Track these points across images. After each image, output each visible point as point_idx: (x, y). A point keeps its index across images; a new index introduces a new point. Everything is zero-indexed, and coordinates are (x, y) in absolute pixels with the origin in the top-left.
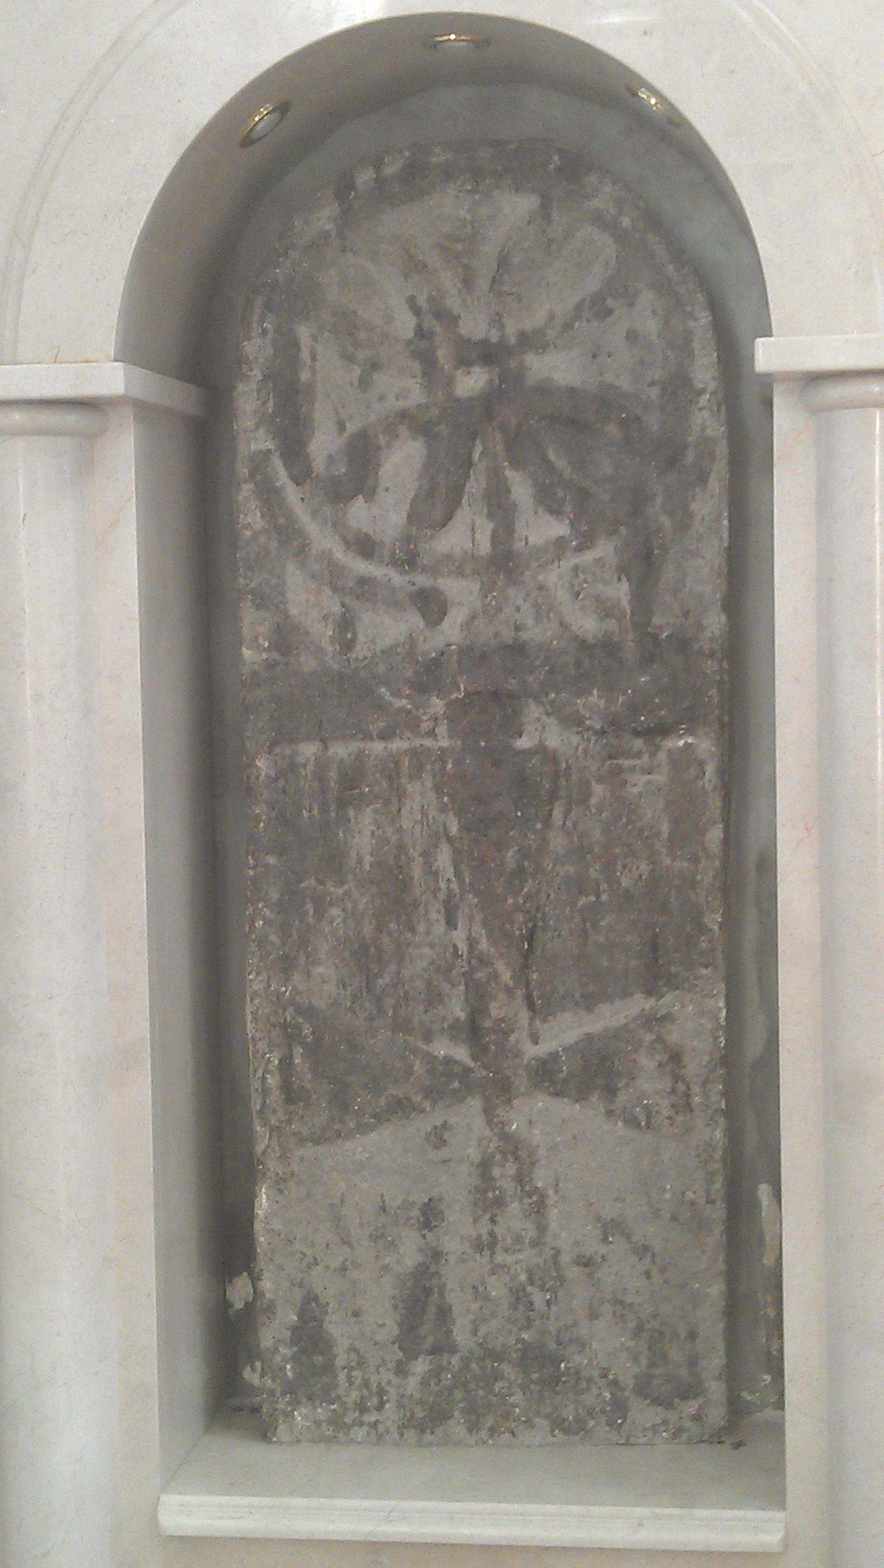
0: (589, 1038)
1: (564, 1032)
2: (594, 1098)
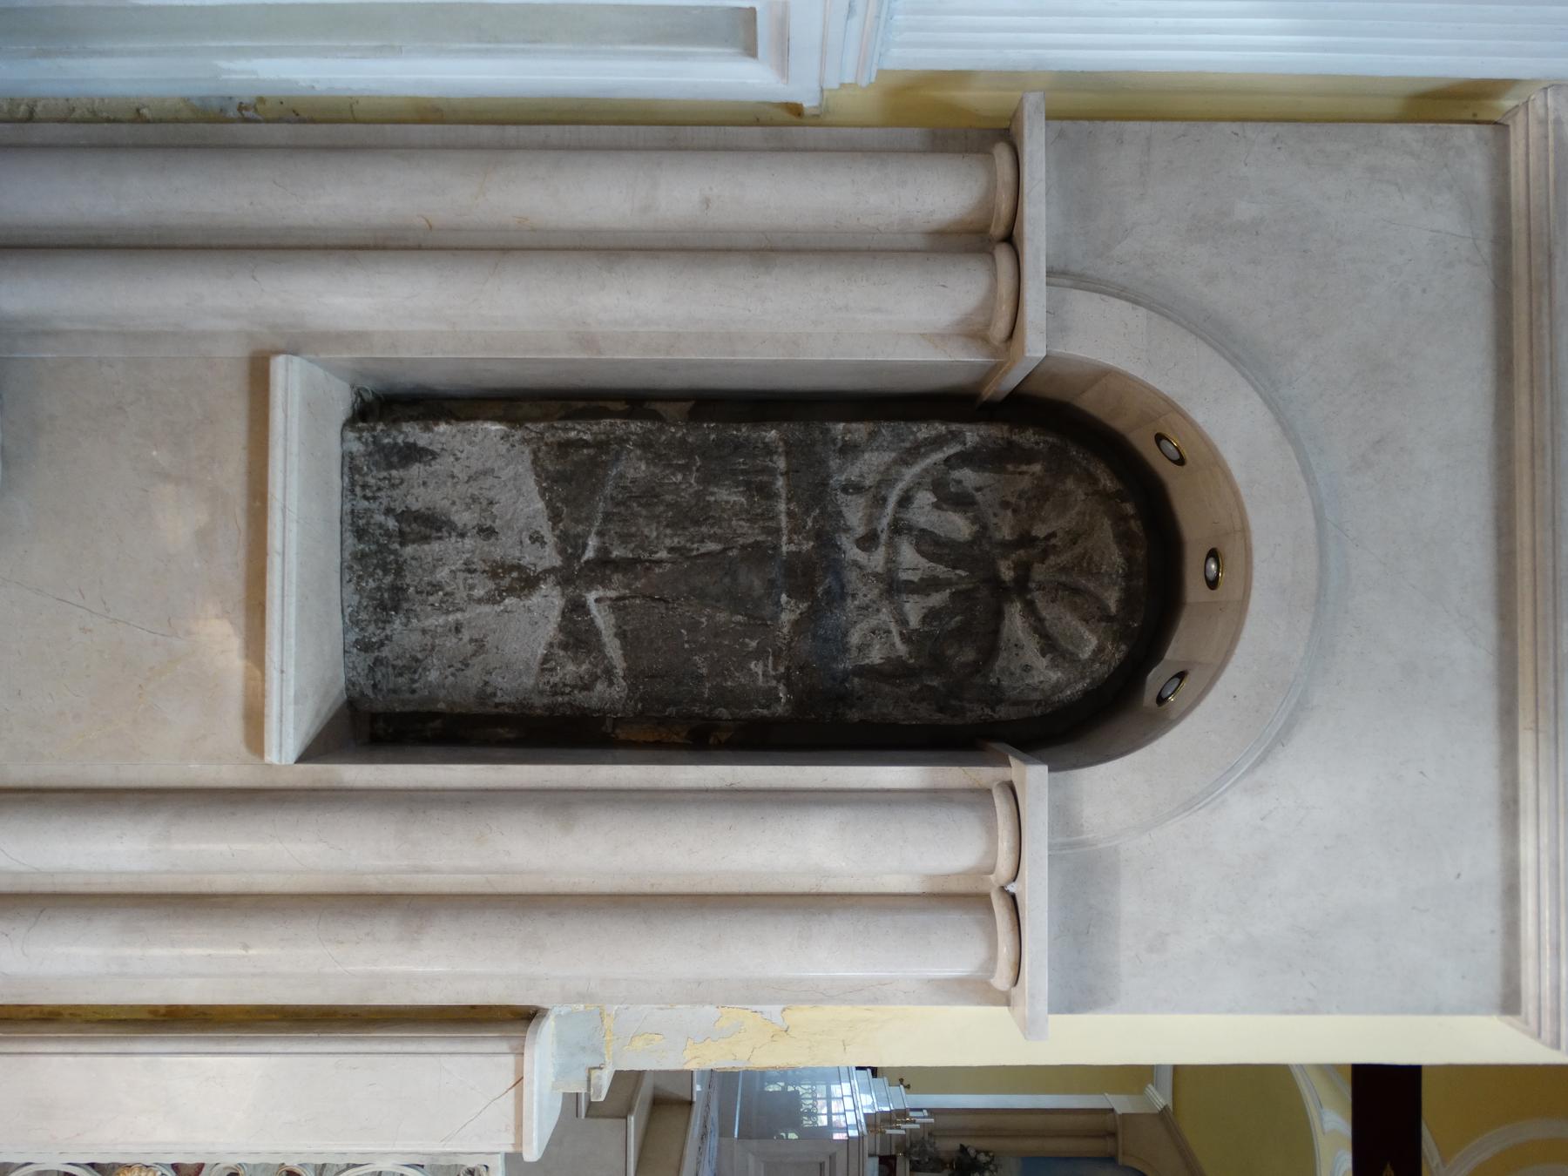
0: (598, 633)
1: (603, 619)
2: (561, 636)
